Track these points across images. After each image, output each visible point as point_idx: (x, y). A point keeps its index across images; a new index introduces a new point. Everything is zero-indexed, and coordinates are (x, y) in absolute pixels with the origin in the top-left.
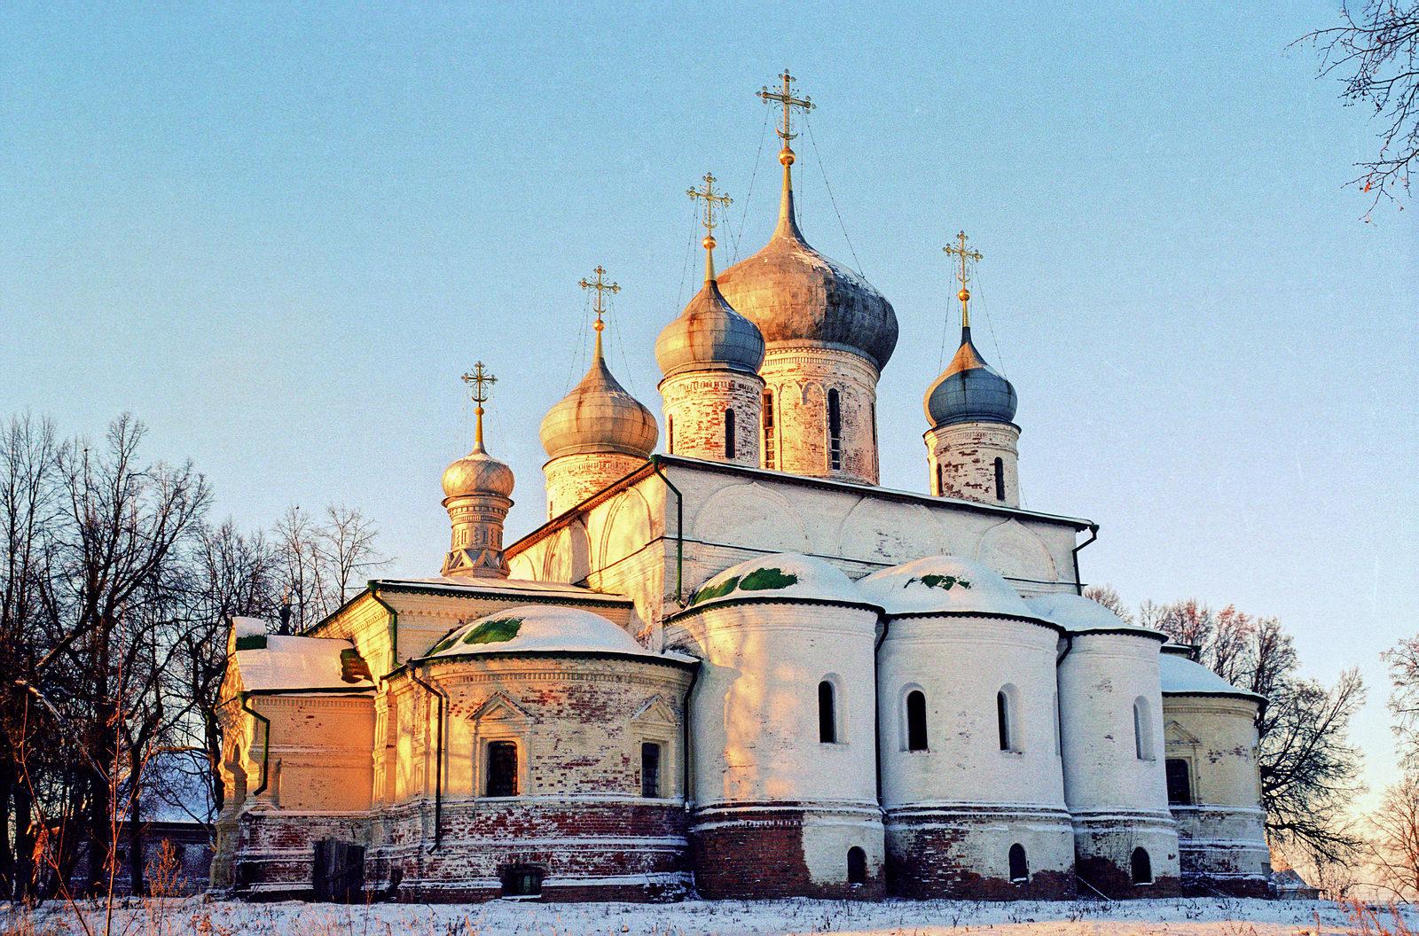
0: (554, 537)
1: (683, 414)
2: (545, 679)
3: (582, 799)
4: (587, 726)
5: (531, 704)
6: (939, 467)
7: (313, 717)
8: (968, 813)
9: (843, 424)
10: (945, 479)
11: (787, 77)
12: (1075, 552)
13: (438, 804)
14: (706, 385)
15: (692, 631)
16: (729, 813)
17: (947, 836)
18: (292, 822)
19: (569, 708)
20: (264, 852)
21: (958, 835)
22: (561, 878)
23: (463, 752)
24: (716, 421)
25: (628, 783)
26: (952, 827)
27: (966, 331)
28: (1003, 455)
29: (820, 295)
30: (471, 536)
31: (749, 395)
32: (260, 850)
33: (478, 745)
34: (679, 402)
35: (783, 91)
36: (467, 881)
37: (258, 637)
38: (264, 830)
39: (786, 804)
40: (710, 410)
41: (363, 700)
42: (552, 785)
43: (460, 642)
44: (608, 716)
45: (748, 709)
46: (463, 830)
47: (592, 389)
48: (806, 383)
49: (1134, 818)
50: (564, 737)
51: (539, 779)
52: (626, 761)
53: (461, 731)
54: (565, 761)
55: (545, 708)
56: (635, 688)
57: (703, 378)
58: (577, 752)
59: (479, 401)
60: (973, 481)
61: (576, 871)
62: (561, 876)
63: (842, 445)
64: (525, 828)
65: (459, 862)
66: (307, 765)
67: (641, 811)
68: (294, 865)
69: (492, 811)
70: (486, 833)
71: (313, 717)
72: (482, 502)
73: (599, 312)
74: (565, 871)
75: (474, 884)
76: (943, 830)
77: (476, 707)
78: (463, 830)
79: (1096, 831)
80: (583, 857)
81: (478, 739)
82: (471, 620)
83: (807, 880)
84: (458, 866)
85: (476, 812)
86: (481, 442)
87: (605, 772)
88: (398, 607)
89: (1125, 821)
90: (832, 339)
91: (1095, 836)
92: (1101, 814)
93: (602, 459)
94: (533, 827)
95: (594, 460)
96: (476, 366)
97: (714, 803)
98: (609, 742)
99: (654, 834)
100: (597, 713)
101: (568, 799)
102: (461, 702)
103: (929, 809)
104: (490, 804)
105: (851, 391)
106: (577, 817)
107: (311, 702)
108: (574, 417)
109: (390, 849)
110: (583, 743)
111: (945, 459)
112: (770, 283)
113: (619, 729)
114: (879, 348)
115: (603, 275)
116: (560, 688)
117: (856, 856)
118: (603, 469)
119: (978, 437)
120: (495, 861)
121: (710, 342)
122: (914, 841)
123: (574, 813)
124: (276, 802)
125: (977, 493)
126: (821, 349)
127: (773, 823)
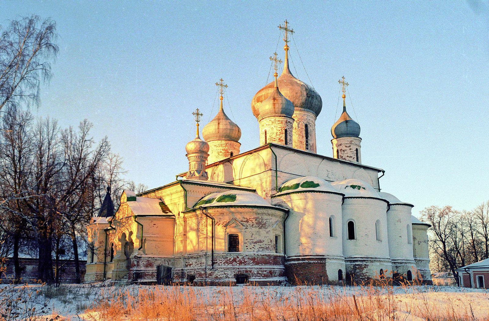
0: (216, 167)
2: (249, 214)
3: (260, 253)
4: (261, 230)
5: (244, 222)
6: (338, 151)
7: (155, 224)
8: (369, 259)
9: (309, 135)
10: (340, 154)
11: (287, 22)
12: (378, 179)
13: (212, 254)
14: (279, 121)
15: (284, 200)
16: (302, 258)
18: (150, 259)
20: (141, 269)
21: (366, 266)
23: (221, 237)
24: (282, 133)
25: (272, 248)
26: (364, 264)
27: (344, 108)
28: (358, 147)
29: (304, 94)
30: (197, 166)
31: (291, 125)
32: (140, 268)
33: (226, 235)
34: (269, 126)
35: (285, 26)
36: (224, 279)
37: (133, 197)
39: (321, 256)
40: (280, 129)
41: (171, 219)
42: (251, 249)
43: (215, 201)
44: (266, 227)
45: (309, 225)
46: (221, 263)
47: (221, 119)
48: (298, 122)
49: (407, 262)
51: (247, 246)
52: (271, 241)
53: (220, 231)
54: (255, 241)
55: (248, 224)
56: (273, 218)
57: (278, 119)
58: (258, 238)
59: (198, 121)
60: (348, 155)
61: (259, 276)
63: (309, 142)
64: (242, 262)
65: (221, 273)
66: (154, 240)
67: (276, 257)
68: (151, 273)
69: (232, 257)
70: (230, 264)
71: (155, 224)
73: (222, 93)
75: (227, 280)
76: (362, 265)
77: (225, 223)
79: (397, 265)
80: (261, 272)
81: (226, 233)
82: (208, 194)
84: (220, 274)
85: (226, 257)
86: (198, 135)
87: (266, 245)
88: (187, 189)
89: (405, 262)
90: (307, 108)
91: (396, 267)
92: (398, 260)
93: (226, 142)
94: (245, 262)
95: (224, 142)
96: (197, 110)
97: (295, 255)
98: (267, 235)
99: (278, 265)
100: (264, 226)
101: (256, 253)
102: (220, 221)
103: (357, 258)
105: (311, 125)
107: (164, 220)
108: (217, 128)
109: (185, 269)
110: (260, 235)
111: (339, 148)
112: (288, 89)
113: (269, 231)
114: (317, 111)
115: (222, 82)
116: (253, 217)
117: (340, 272)
118: (226, 145)
119: (351, 142)
121: (280, 107)
122: (352, 268)
123: (258, 258)
124: (144, 252)
125: (351, 159)
126: (303, 111)
127: (317, 262)
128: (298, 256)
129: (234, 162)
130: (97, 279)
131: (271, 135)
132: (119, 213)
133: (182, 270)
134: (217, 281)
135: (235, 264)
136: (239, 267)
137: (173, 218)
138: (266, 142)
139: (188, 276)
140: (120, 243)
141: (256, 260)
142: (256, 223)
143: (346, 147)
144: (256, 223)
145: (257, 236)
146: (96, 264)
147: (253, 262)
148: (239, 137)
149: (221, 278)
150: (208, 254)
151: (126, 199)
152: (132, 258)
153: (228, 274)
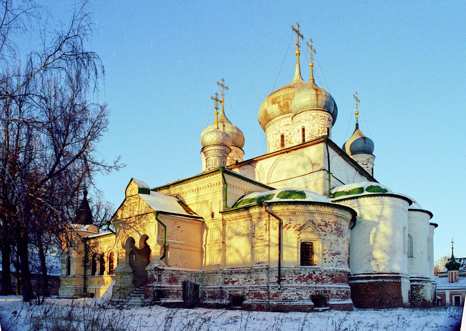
1: (311, 126)
4: (339, 238)
17: (420, 287)
18: (174, 273)
19: (334, 230)
22: (334, 301)
24: (324, 131)
27: (357, 125)
32: (178, 285)
36: (296, 301)
38: (163, 275)
40: (323, 126)
42: (329, 262)
46: (292, 280)
50: (333, 242)
51: (325, 259)
54: (334, 252)
61: (338, 298)
62: (333, 300)
64: (320, 280)
65: (292, 293)
66: (178, 248)
68: (176, 291)
69: (306, 272)
70: (303, 281)
72: (224, 149)
74: (335, 298)
75: (301, 303)
76: (418, 285)
77: (298, 227)
78: (292, 280)
81: (299, 240)
83: (402, 301)
84: (291, 295)
88: (227, 182)
94: (323, 279)
102: (290, 223)
104: (306, 269)
106: (336, 276)
109: (225, 287)
119: (368, 159)
120: (309, 294)
121: (324, 100)
123: (336, 274)
128: (368, 274)
129: (257, 164)
130: (76, 293)
131: (312, 132)
132: (122, 210)
133: (221, 288)
134: (287, 304)
135: (311, 282)
136: (316, 286)
137: (201, 221)
138: (304, 140)
139: (230, 295)
140: (124, 251)
141: (334, 277)
142: (335, 229)
143: (363, 164)
144: (335, 229)
145: (336, 246)
146: (74, 277)
147: (331, 280)
148: (243, 145)
149: (291, 300)
150: (272, 268)
151: (137, 190)
152: (150, 271)
153: (302, 295)
